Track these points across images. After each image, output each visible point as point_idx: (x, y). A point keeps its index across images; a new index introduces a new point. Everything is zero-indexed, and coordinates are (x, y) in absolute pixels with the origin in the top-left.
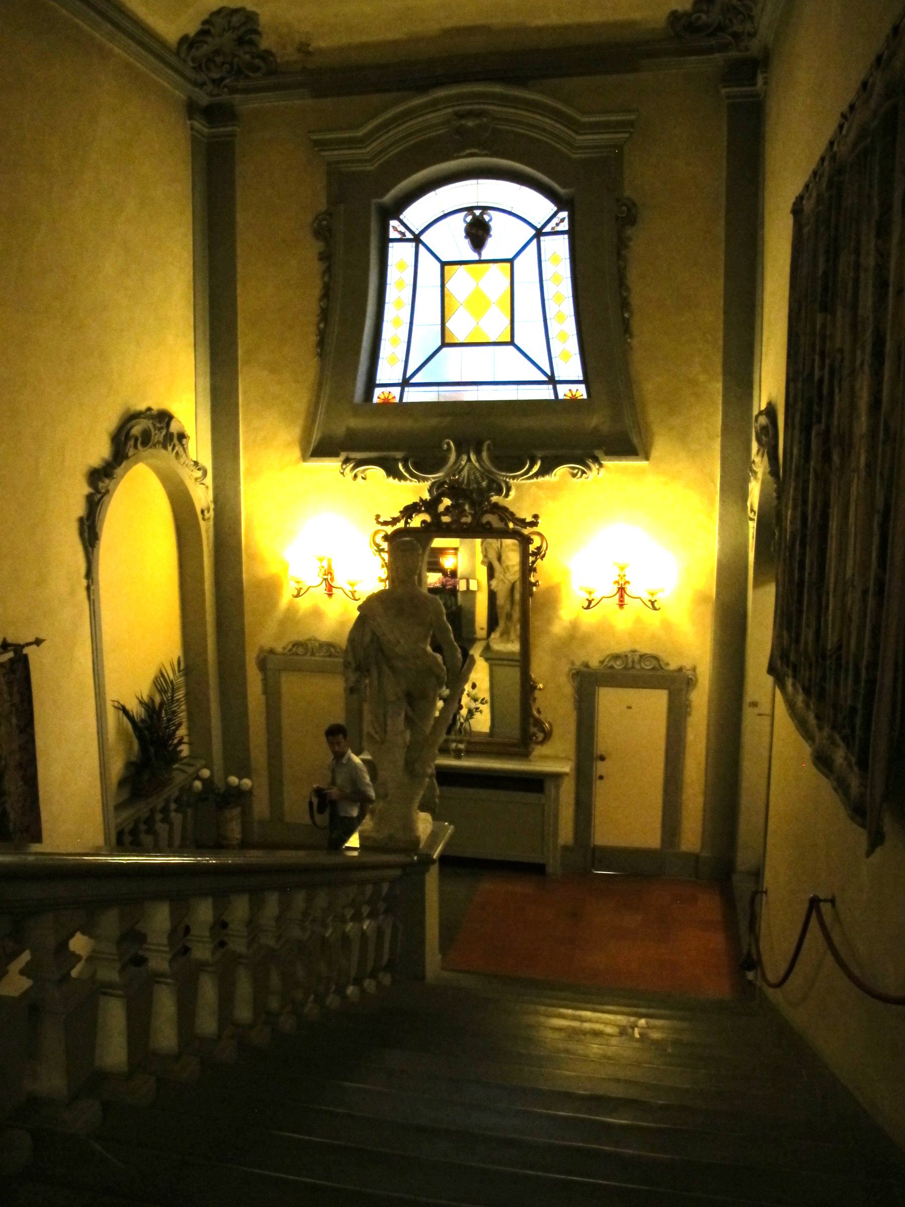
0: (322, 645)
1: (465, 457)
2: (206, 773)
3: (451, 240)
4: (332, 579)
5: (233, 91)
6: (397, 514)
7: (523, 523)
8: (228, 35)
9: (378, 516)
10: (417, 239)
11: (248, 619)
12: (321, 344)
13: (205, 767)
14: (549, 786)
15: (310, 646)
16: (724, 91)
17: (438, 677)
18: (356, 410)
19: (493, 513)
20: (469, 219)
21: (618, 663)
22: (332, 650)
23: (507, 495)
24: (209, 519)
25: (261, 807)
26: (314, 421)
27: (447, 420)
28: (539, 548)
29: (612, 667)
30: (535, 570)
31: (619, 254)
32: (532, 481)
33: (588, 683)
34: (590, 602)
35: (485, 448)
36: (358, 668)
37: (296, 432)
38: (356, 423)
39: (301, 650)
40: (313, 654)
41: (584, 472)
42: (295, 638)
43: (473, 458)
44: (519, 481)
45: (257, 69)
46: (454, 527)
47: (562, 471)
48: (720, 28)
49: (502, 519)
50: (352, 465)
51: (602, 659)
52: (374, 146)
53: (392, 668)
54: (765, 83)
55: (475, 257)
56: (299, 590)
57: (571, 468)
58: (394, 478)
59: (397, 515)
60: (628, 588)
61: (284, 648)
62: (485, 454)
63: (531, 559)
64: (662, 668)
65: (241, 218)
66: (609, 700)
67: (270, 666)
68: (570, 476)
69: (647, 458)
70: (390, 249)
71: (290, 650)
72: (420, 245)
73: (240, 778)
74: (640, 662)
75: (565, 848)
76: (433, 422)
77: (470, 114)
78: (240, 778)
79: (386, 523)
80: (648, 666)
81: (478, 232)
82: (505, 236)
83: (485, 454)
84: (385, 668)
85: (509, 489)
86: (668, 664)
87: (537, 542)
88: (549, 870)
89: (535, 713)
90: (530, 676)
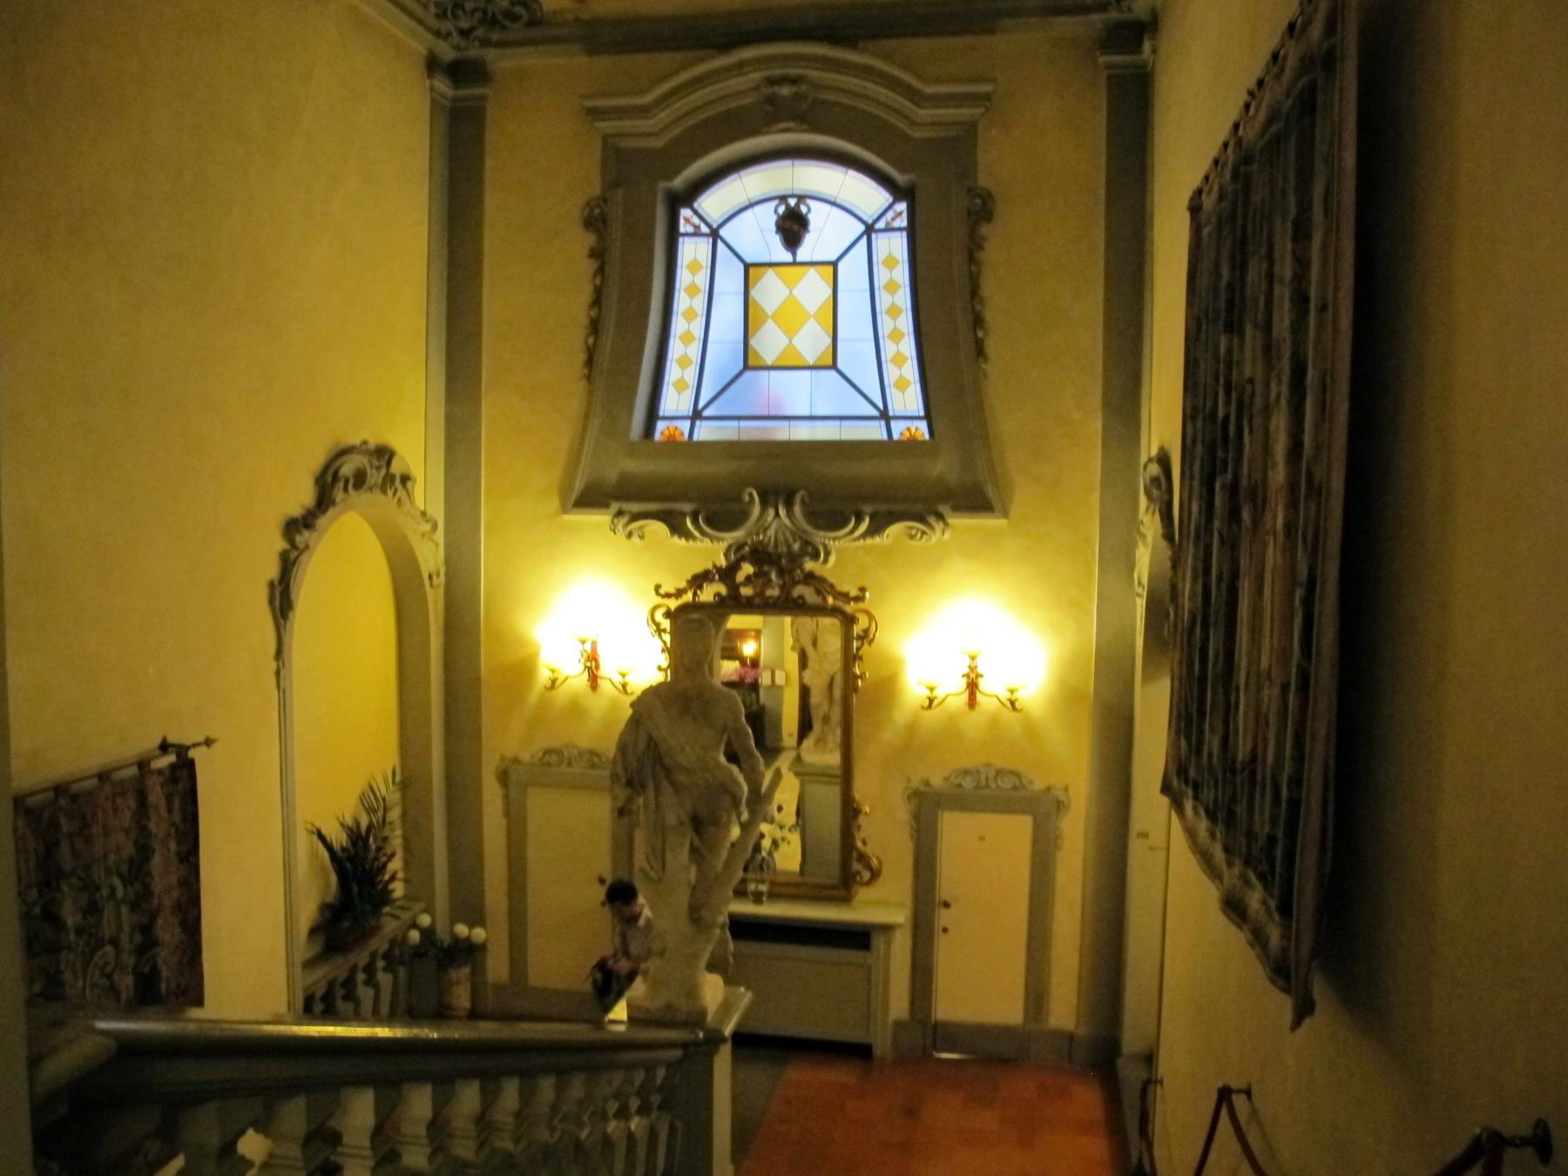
0: (581, 754)
1: (771, 512)
2: (425, 920)
3: (756, 233)
4: (597, 667)
5: (486, 43)
7: (845, 597)
12: (590, 362)
13: (425, 911)
14: (878, 941)
16: (1102, 59)
18: (632, 450)
20: (782, 209)
21: (968, 779)
25: (497, 967)
26: (577, 461)
28: (866, 631)
29: (960, 786)
33: (927, 808)
34: (931, 701)
35: (798, 499)
36: (630, 783)
37: (555, 475)
39: (554, 759)
40: (570, 764)
41: (924, 533)
43: (782, 512)
44: (844, 544)
46: (757, 601)
47: (896, 529)
49: (818, 592)
52: (664, 116)
53: (674, 784)
56: (554, 681)
59: (683, 585)
62: (797, 509)
66: (954, 828)
67: (513, 778)
69: (1005, 515)
75: (898, 1024)
76: (733, 465)
79: (668, 596)
80: (1006, 784)
81: (792, 227)
82: (828, 233)
83: (797, 509)
84: (665, 783)
85: (827, 554)
87: (863, 622)
88: (877, 1052)
89: (859, 844)
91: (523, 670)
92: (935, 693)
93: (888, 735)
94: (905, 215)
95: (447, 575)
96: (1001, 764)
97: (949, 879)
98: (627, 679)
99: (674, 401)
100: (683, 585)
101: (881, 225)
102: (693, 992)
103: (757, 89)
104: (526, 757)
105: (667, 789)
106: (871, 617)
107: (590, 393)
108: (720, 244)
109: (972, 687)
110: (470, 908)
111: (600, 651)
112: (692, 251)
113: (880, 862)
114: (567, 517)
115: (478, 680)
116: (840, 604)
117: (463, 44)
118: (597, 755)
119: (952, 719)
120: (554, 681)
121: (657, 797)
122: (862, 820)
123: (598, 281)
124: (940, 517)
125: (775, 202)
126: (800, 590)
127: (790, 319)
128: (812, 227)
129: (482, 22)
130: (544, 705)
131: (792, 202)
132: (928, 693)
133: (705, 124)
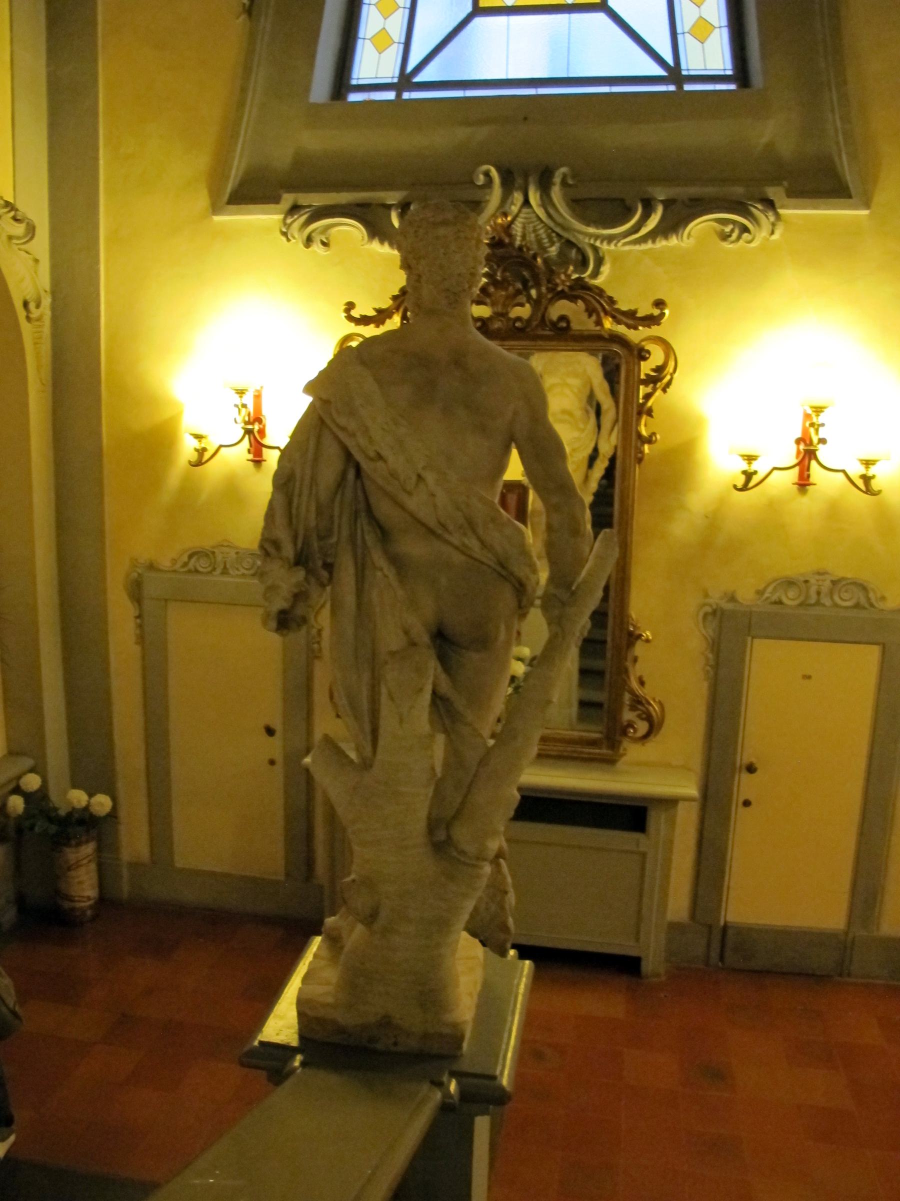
1: (518, 197)
2: (32, 782)
4: (262, 432)
6: (386, 303)
7: (632, 318)
9: (350, 306)
11: (110, 506)
13: (32, 770)
14: (656, 820)
15: (219, 558)
17: (520, 589)
18: (314, 116)
19: (573, 299)
21: (792, 594)
23: (596, 274)
24: (39, 319)
25: (134, 842)
26: (234, 136)
27: (482, 133)
28: (660, 369)
29: (780, 602)
30: (650, 413)
32: (643, 247)
33: (730, 633)
34: (749, 475)
35: (557, 179)
36: (301, 560)
37: (200, 162)
38: (315, 141)
39: (202, 564)
40: (225, 572)
41: (745, 229)
43: (534, 197)
44: (622, 247)
46: (497, 325)
47: (702, 226)
49: (590, 311)
51: (761, 587)
53: (397, 562)
56: (201, 452)
57: (718, 221)
58: (382, 242)
60: (822, 452)
61: (174, 561)
62: (556, 193)
63: (643, 390)
64: (872, 605)
66: (771, 665)
68: (716, 239)
69: (867, 205)
71: (185, 564)
73: (91, 795)
74: (831, 593)
75: (675, 928)
76: (461, 133)
78: (91, 795)
79: (364, 320)
80: (846, 599)
83: (556, 193)
84: (378, 558)
85: (599, 262)
86: (883, 598)
87: (657, 357)
88: (647, 967)
89: (634, 684)
90: (629, 616)
91: (158, 441)
92: (755, 466)
93: (681, 529)
95: (54, 308)
96: (840, 573)
97: (757, 736)
99: (374, 64)
102: (431, 993)
104: (165, 563)
105: (383, 571)
106: (668, 349)
107: (252, 37)
109: (808, 454)
110: (94, 769)
111: (266, 412)
113: (661, 704)
114: (217, 218)
115: (98, 454)
116: (621, 329)
119: (773, 505)
120: (201, 452)
121: (360, 591)
122: (639, 649)
124: (770, 204)
126: (560, 308)
130: (188, 491)
132: (744, 466)
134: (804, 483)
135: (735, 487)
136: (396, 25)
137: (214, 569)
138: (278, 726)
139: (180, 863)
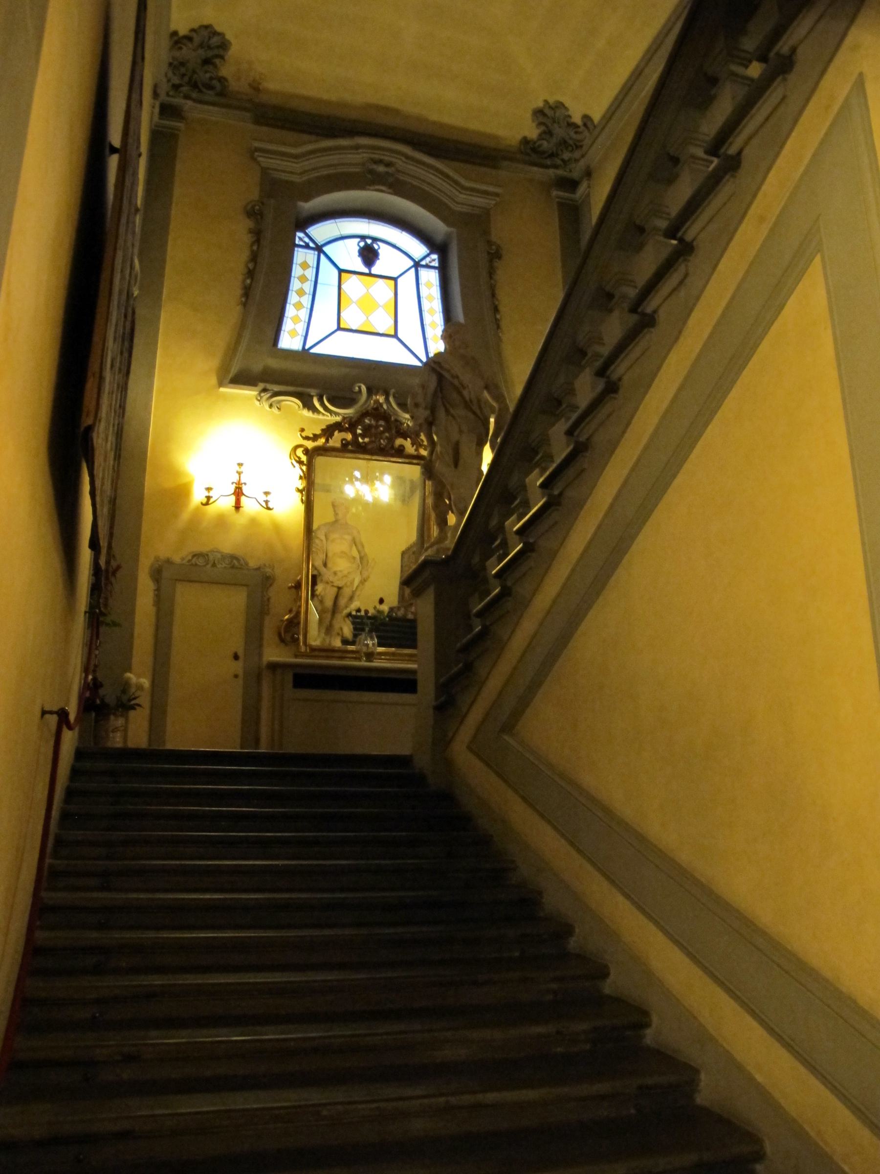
0: (224, 557)
3: (347, 254)
5: (187, 97)
8: (201, 51)
10: (319, 249)
12: (247, 292)
15: (211, 558)
16: (555, 193)
20: (362, 244)
22: (235, 561)
31: (491, 278)
37: (214, 363)
39: (201, 561)
42: (197, 549)
45: (211, 88)
48: (552, 155)
50: (269, 395)
52: (307, 164)
54: (589, 187)
55: (366, 271)
59: (318, 432)
62: (391, 399)
65: (178, 191)
67: (165, 574)
70: (296, 253)
71: (189, 561)
72: (322, 256)
76: (345, 370)
77: (380, 162)
81: (369, 255)
82: (389, 261)
91: (181, 493)
93: (185, 516)
94: (437, 261)
98: (269, 498)
99: (289, 341)
100: (318, 432)
101: (423, 263)
103: (363, 164)
104: (177, 559)
108: (322, 256)
112: (300, 256)
114: (222, 389)
117: (171, 93)
118: (237, 559)
123: (255, 248)
125: (358, 240)
127: (368, 304)
128: (380, 257)
129: (189, 83)
131: (369, 241)
133: (329, 177)
134: (238, 507)
135: (202, 504)
136: (301, 328)
137: (207, 564)
138: (241, 653)
139: (701, 1099)
